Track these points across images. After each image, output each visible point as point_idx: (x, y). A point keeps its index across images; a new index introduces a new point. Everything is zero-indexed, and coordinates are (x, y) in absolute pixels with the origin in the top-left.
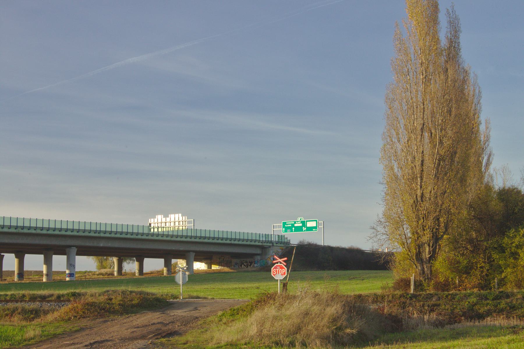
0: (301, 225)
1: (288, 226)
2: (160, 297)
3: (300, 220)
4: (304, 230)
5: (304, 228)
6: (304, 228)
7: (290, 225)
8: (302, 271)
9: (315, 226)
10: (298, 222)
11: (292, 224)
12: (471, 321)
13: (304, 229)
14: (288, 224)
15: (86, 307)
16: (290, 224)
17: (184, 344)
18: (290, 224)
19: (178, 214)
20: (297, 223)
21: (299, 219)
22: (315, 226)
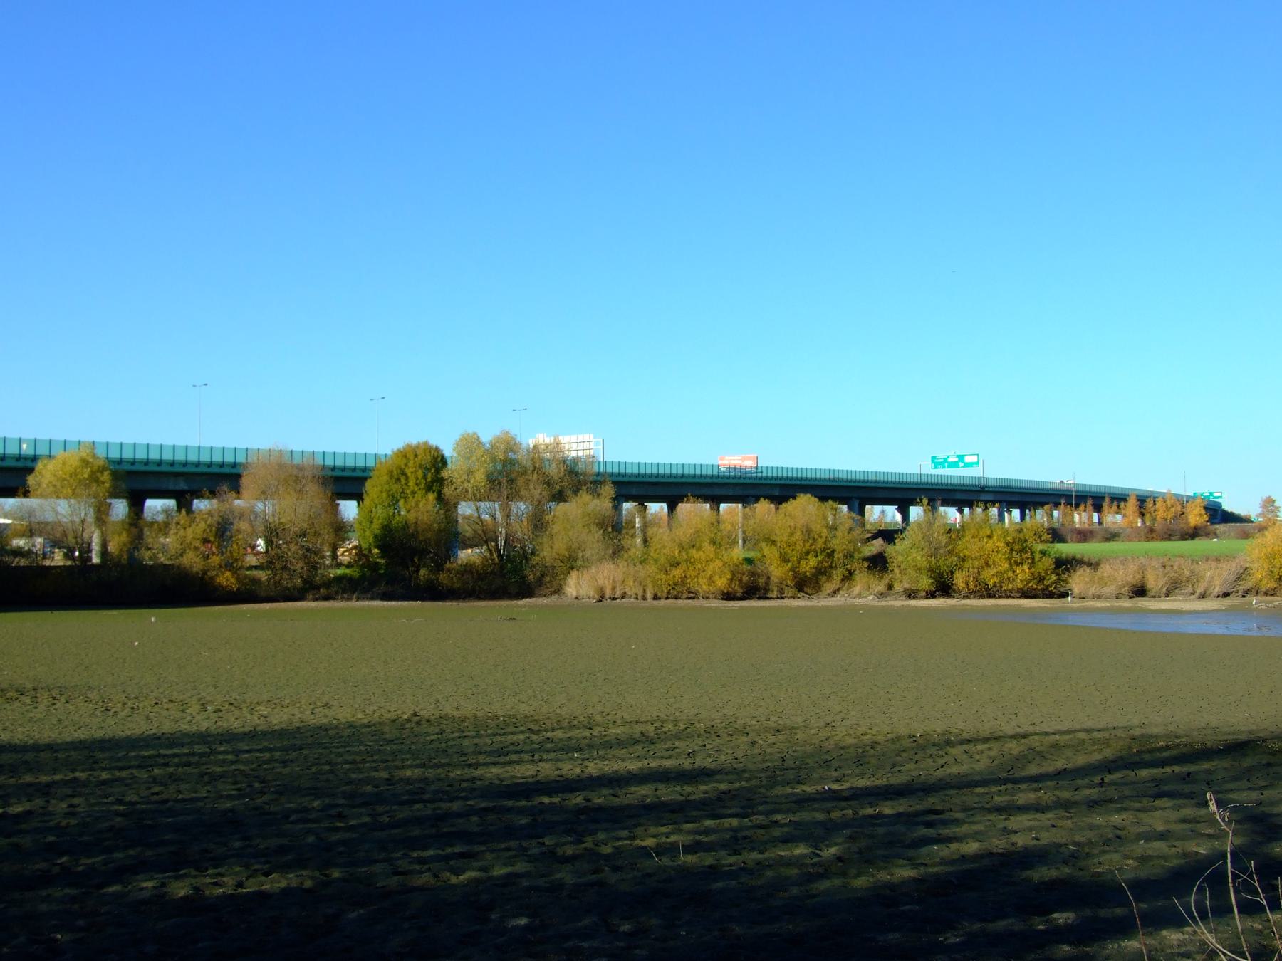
0: (957, 460)
7: (942, 460)
13: (961, 464)
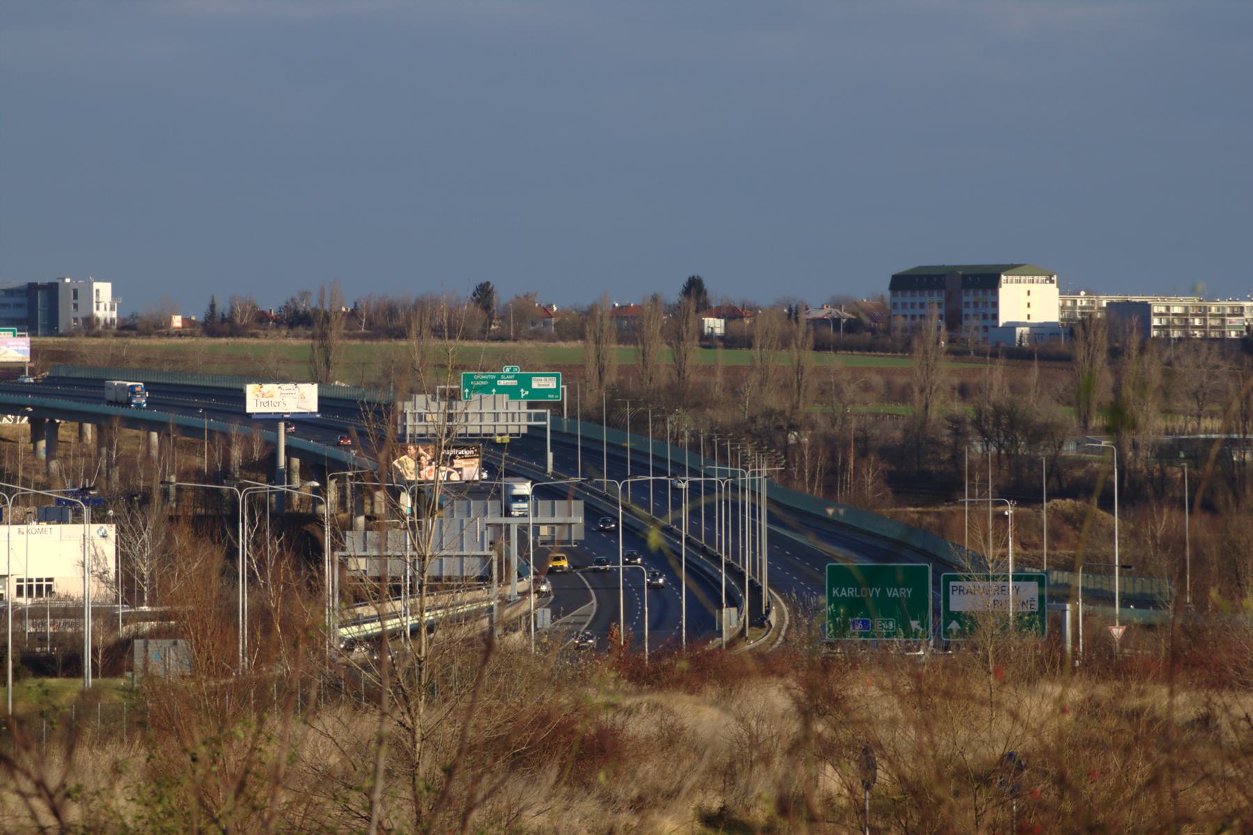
0: (515, 382)
1: (478, 383)
2: (454, 794)
3: (511, 370)
4: (523, 395)
5: (522, 390)
6: (522, 390)
8: (648, 691)
9: (555, 387)
10: (506, 375)
11: (489, 380)
12: (105, 320)
14: (479, 380)
15: (330, 667)
16: (484, 380)
17: (116, 403)
18: (484, 380)
19: (549, 502)
20: (503, 377)
21: (508, 370)
22: (555, 387)
